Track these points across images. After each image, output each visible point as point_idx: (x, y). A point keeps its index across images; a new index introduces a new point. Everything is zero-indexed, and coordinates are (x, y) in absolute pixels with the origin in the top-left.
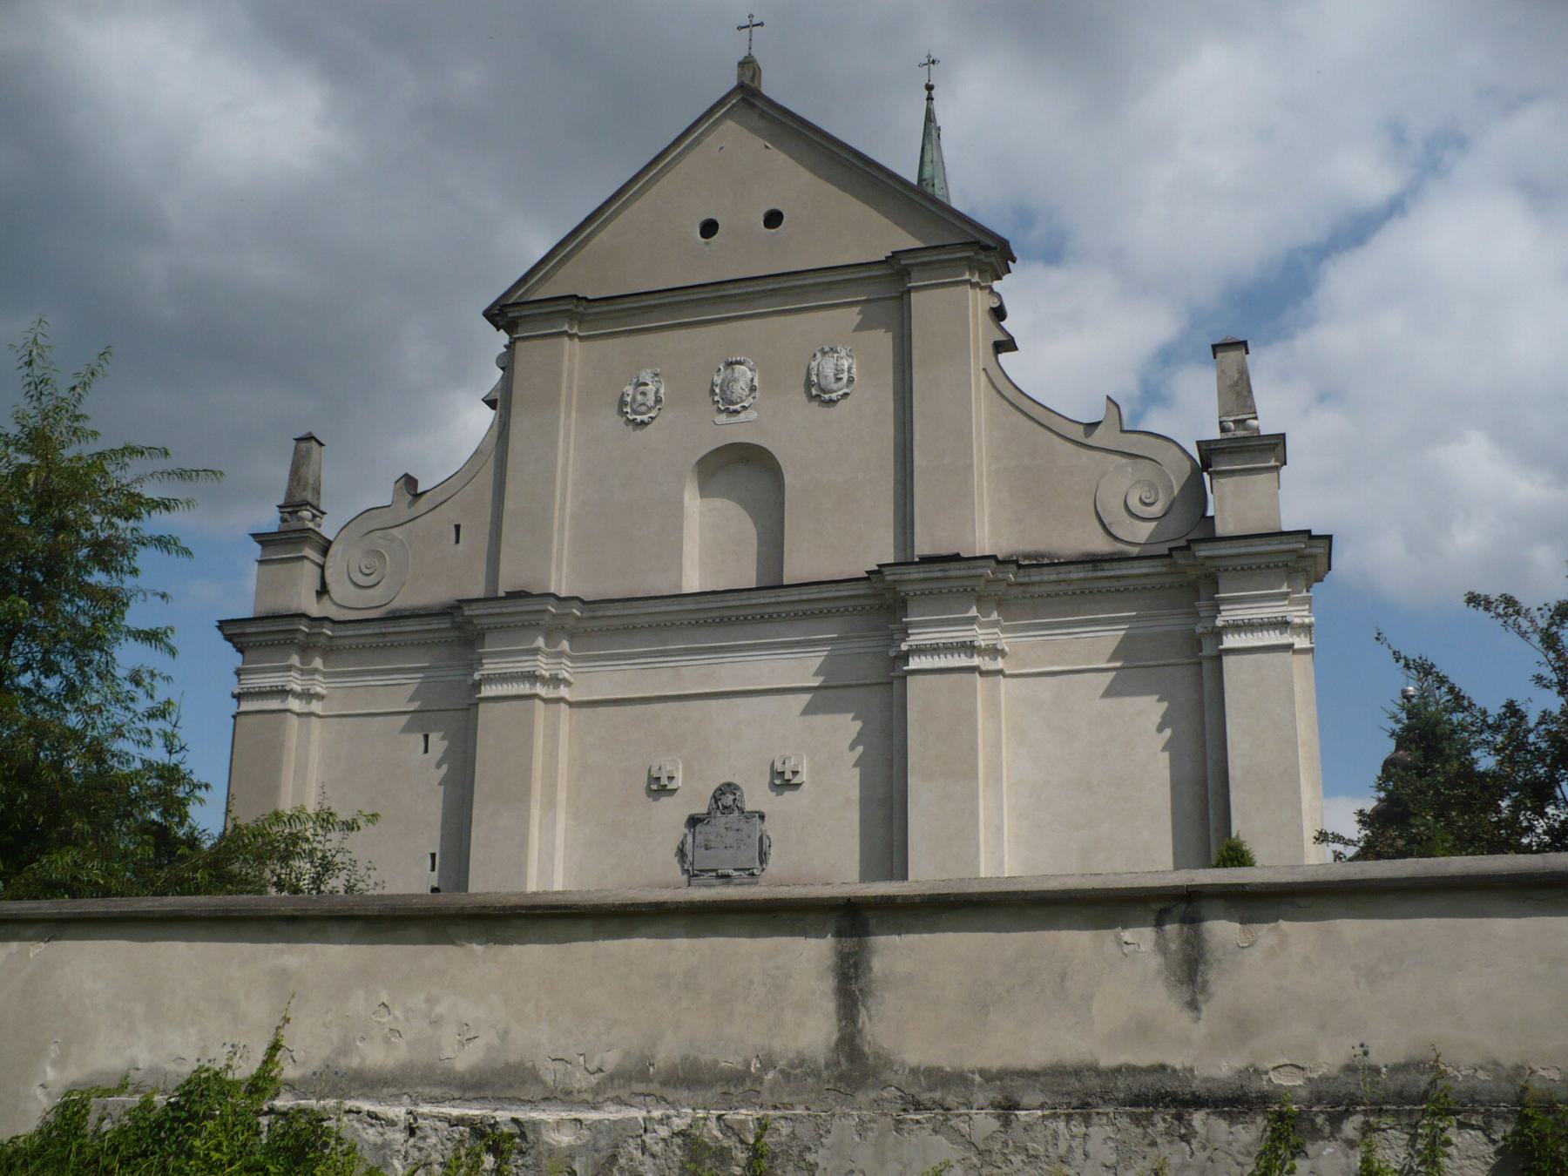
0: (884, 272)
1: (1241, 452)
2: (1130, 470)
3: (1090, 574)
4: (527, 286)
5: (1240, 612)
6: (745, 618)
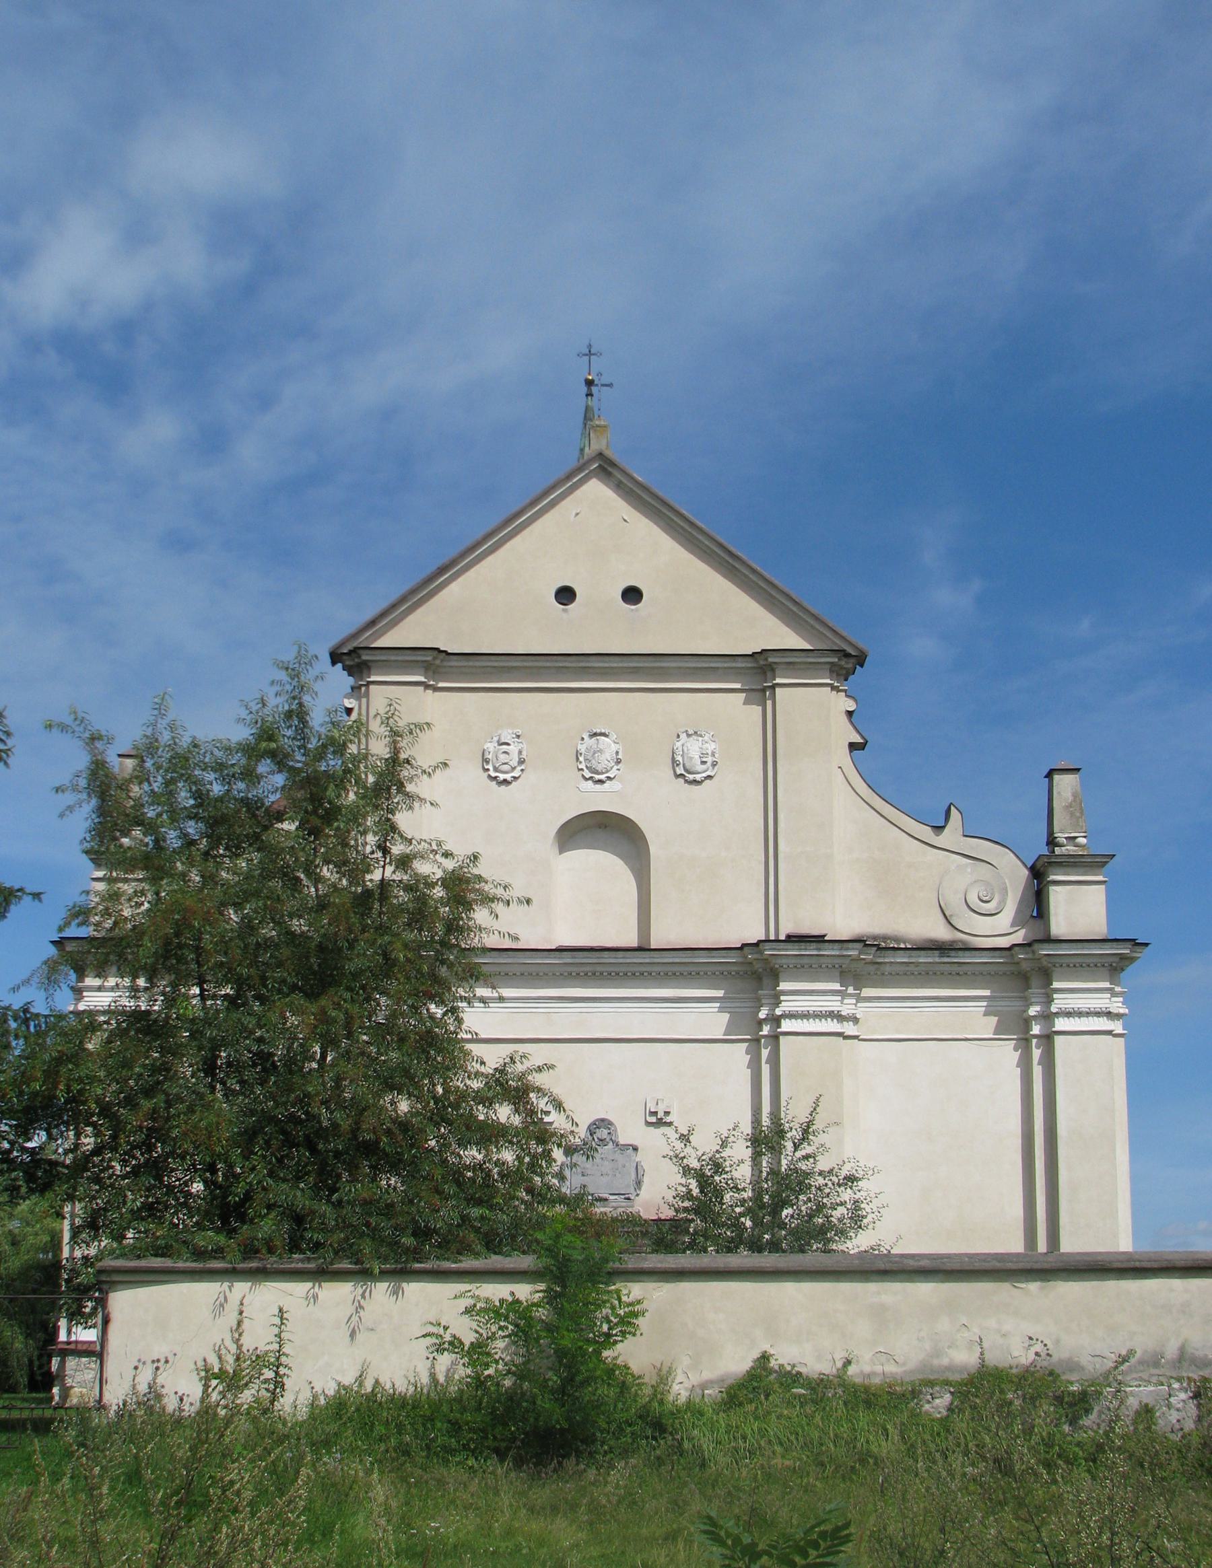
0: (750, 665)
1: (1076, 866)
2: (969, 870)
3: (937, 960)
4: (374, 629)
5: (1069, 1001)
6: (578, 974)
